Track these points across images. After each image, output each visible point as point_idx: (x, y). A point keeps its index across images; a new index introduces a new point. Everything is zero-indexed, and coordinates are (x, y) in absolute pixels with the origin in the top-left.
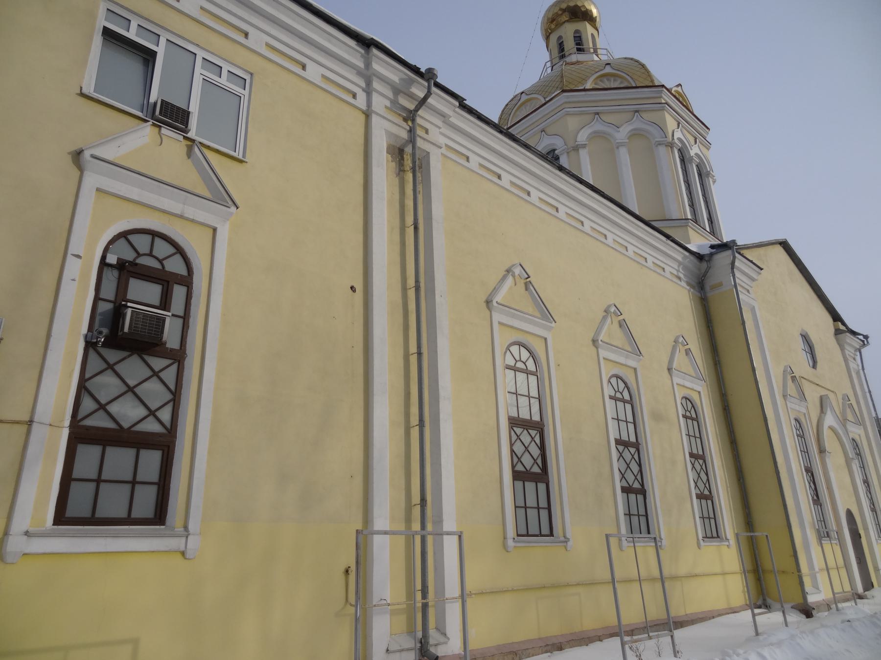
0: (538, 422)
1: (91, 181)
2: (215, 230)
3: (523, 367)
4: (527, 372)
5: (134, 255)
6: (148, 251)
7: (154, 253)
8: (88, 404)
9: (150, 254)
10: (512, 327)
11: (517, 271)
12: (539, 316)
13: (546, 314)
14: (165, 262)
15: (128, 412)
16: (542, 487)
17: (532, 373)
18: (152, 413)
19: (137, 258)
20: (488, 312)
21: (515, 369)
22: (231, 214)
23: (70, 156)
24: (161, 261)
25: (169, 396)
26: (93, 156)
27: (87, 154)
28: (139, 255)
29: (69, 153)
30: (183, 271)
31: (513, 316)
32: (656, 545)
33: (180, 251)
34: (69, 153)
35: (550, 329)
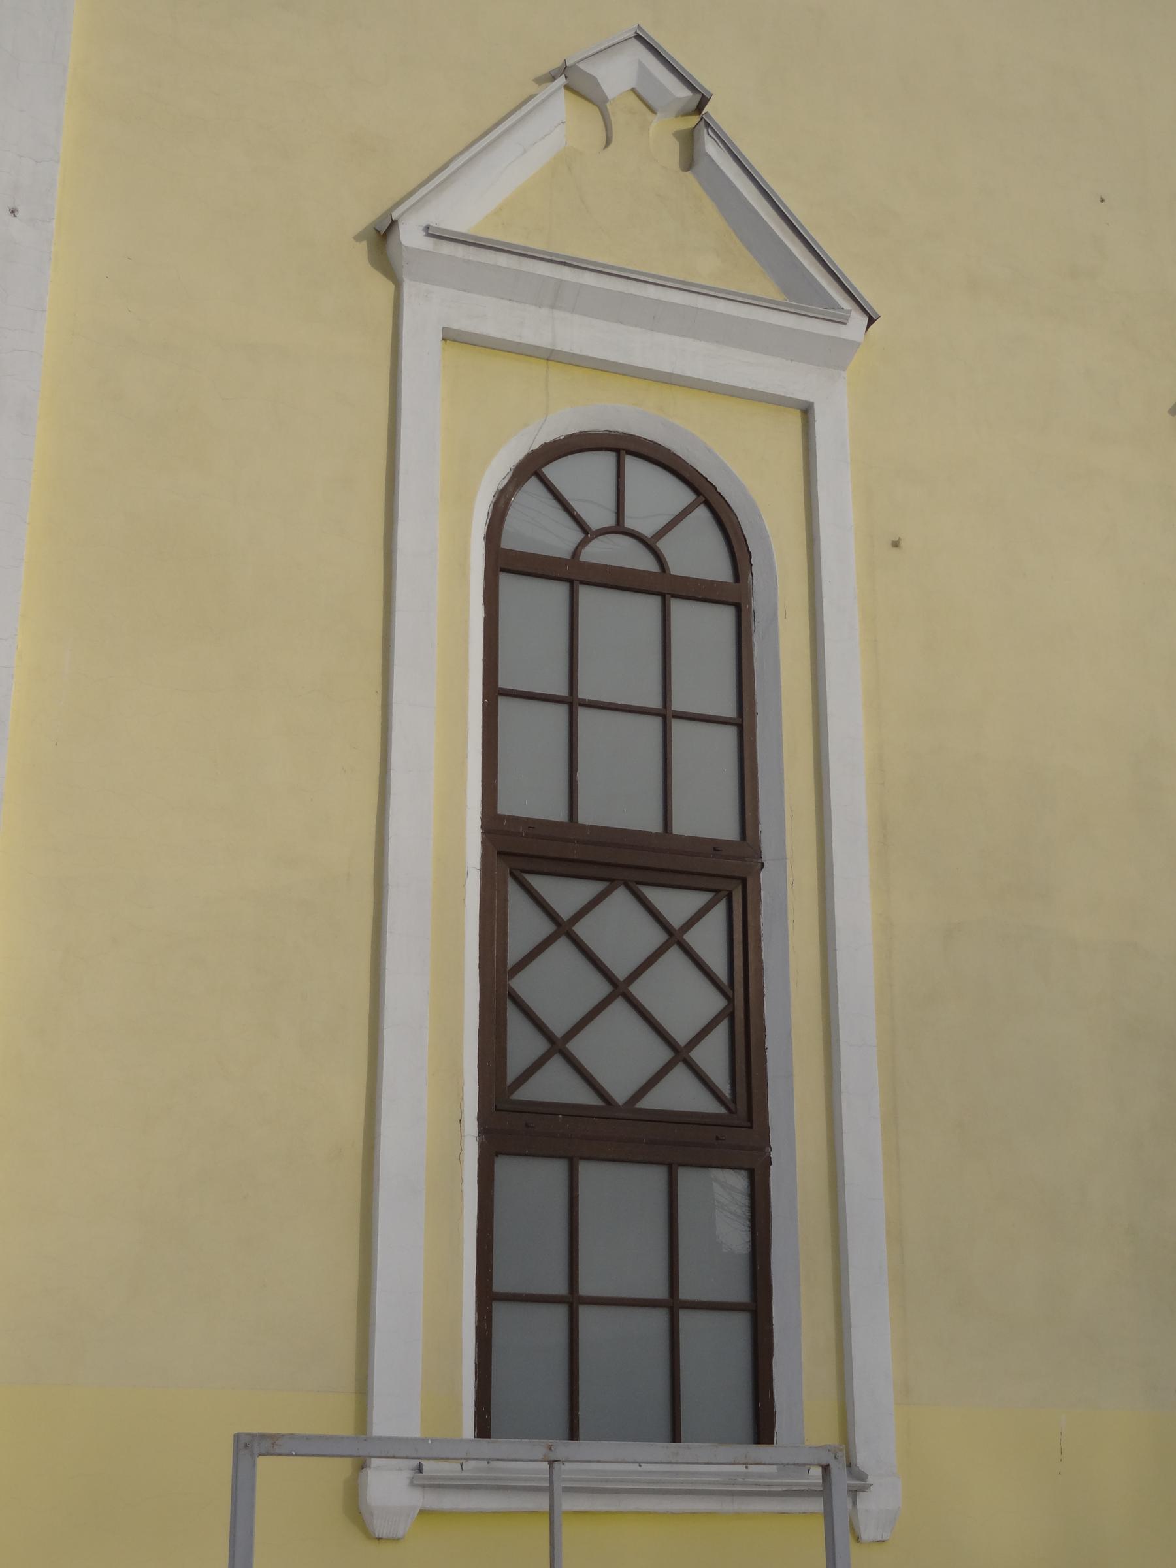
0: (716, 847)
1: (429, 308)
2: (807, 412)
3: (647, 564)
4: (666, 588)
5: (576, 536)
6: (609, 520)
7: (629, 523)
8: (523, 1045)
9: (619, 528)
10: (550, 356)
11: (617, 75)
12: (772, 292)
13: (808, 280)
14: (663, 545)
15: (619, 1057)
16: (726, 1188)
17: (700, 592)
18: (680, 1055)
19: (583, 543)
20: (381, 288)
21: (573, 574)
22: (854, 346)
23: (364, 245)
24: (649, 544)
25: (521, 984)
26: (432, 233)
27: (410, 235)
28: (588, 533)
29: (358, 238)
30: (717, 569)
31: (555, 298)
32: (828, 1515)
33: (705, 493)
34: (358, 238)
35: (836, 356)
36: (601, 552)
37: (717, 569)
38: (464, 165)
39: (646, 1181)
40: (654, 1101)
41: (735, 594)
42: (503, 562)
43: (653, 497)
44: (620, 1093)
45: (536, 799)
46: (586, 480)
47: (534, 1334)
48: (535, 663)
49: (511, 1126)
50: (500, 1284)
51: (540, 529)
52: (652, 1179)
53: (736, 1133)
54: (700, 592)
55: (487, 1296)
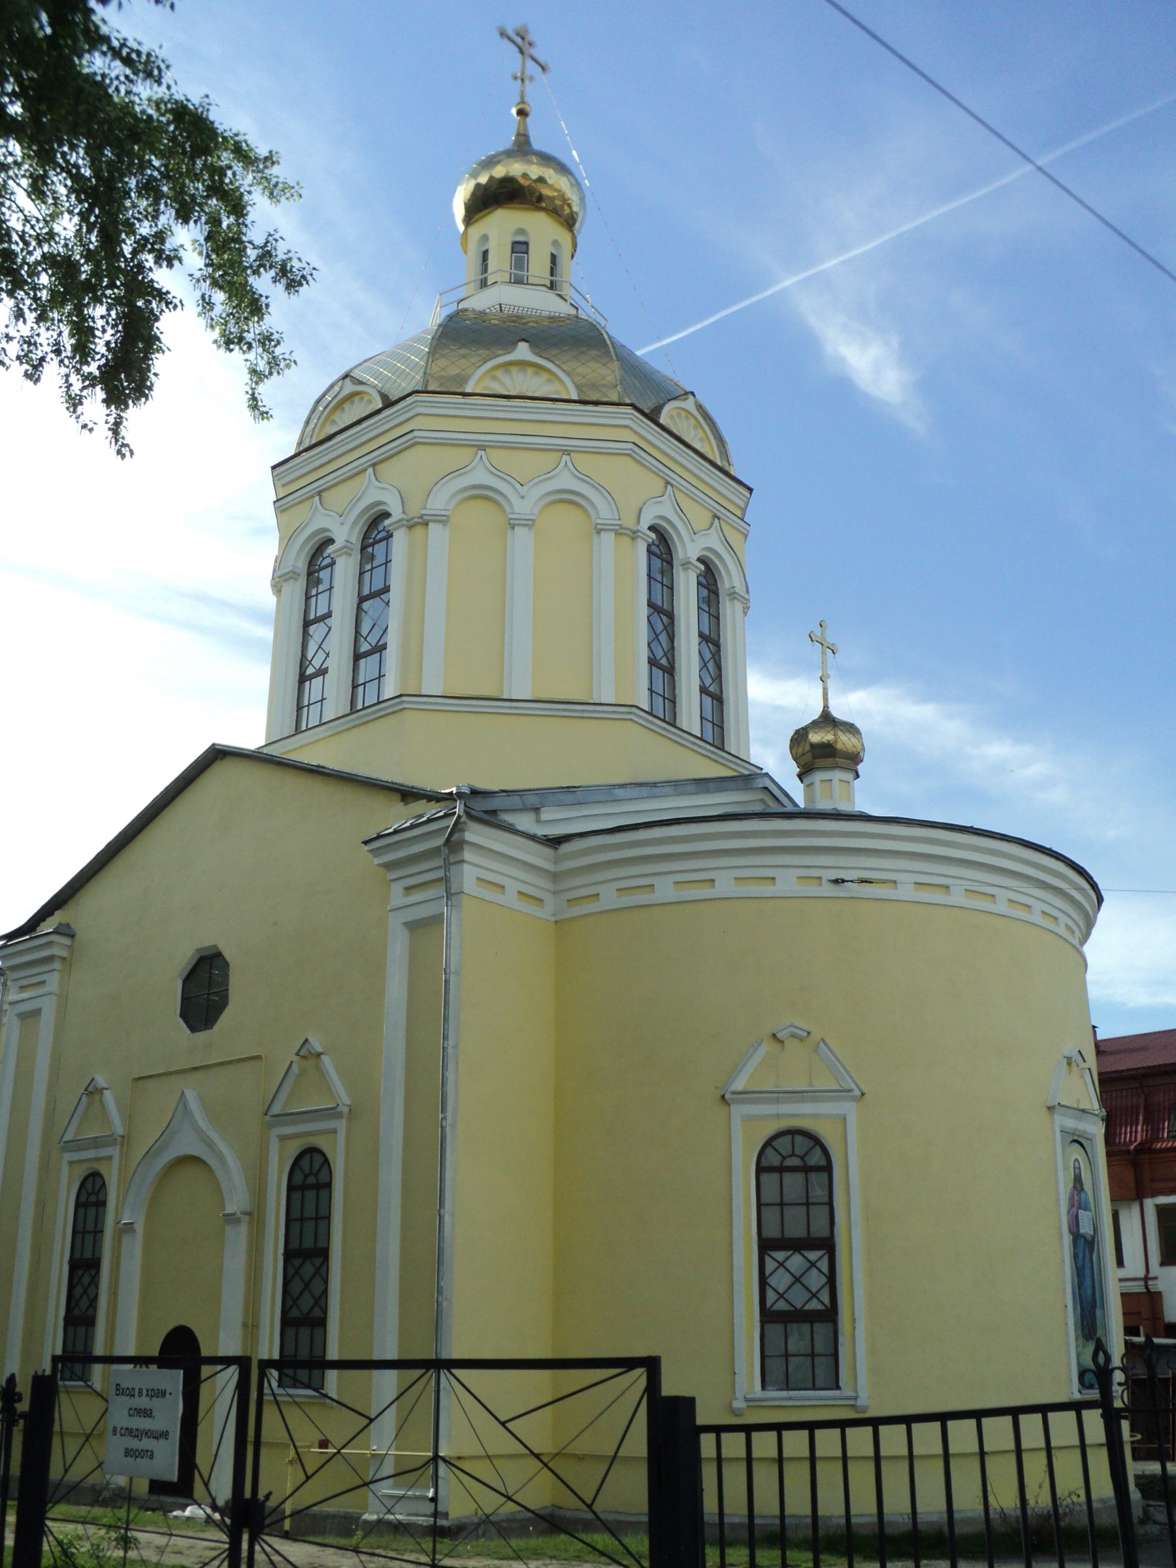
4: (806, 1169)
9: (793, 1155)
17: (817, 1169)
21: (781, 1170)
36: (789, 1162)
37: (823, 1162)
38: (423, 835)
39: (789, 1234)
40: (807, 1308)
41: (828, 1168)
42: (760, 1170)
43: (801, 1143)
44: (799, 1307)
45: (772, 1232)
46: (784, 1144)
47: (776, 1365)
48: (771, 1195)
49: (768, 1316)
50: (763, 1201)
51: (773, 1159)
52: (787, 1235)
53: (830, 1315)
54: (817, 1169)
55: (759, 1205)
